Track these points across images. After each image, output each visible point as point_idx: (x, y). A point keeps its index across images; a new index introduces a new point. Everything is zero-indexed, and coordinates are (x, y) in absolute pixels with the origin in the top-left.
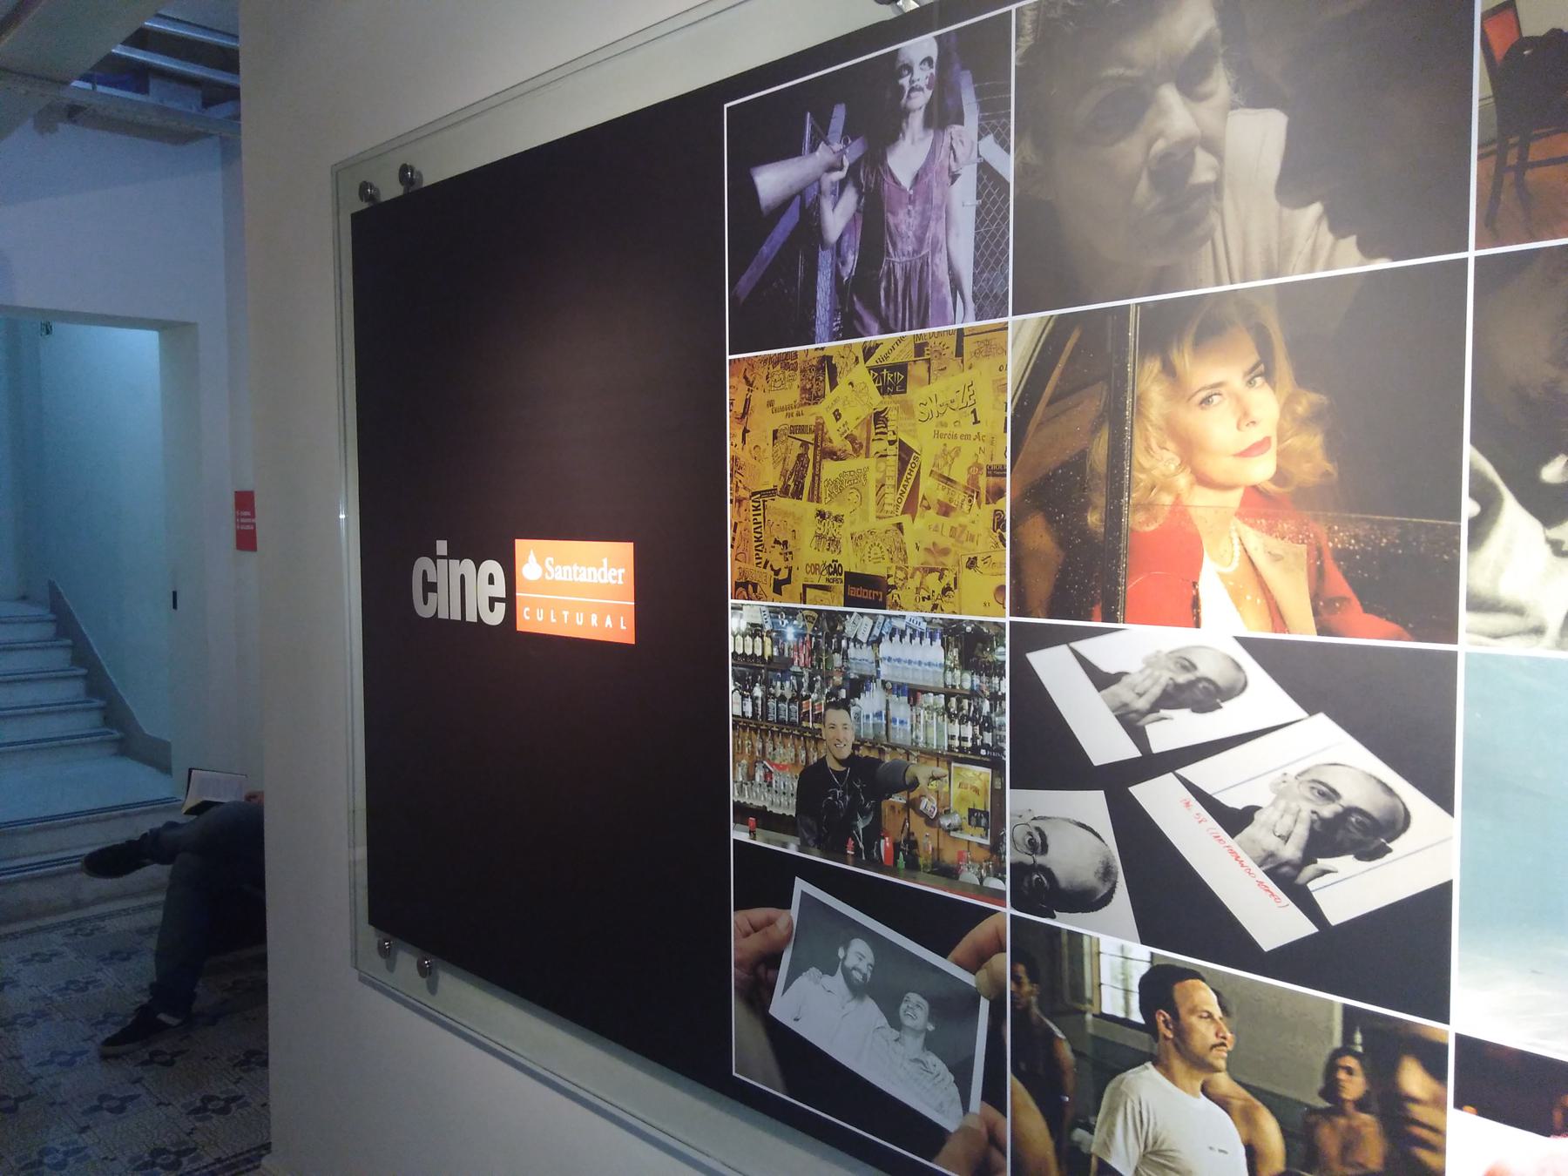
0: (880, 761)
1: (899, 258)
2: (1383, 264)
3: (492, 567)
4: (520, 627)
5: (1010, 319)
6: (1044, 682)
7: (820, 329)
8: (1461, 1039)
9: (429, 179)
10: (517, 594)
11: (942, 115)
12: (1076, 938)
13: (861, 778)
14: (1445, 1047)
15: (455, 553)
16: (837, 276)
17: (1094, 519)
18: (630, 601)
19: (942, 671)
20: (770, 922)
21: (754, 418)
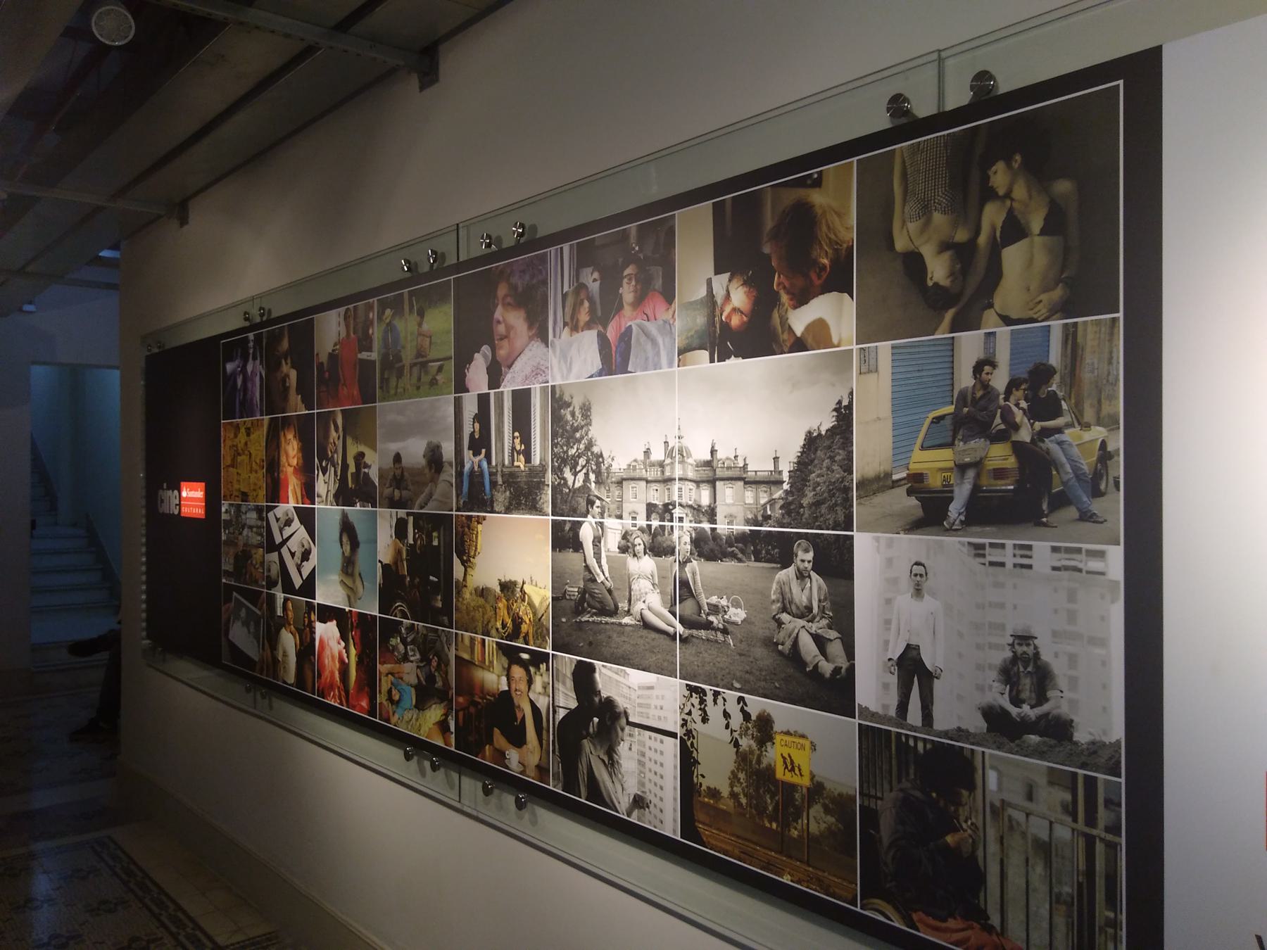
0: (306, 549)
1: (249, 396)
2: (307, 412)
3: (176, 492)
4: (182, 515)
5: (265, 417)
6: (1165, 732)
7: (237, 416)
8: (318, 604)
9: (167, 347)
10: (204, 504)
11: (254, 359)
12: (274, 594)
13: (564, 530)
14: (498, 388)
15: (168, 488)
16: (239, 399)
17: (276, 474)
18: (202, 502)
19: (182, 502)
20: (229, 607)
21: (227, 441)
